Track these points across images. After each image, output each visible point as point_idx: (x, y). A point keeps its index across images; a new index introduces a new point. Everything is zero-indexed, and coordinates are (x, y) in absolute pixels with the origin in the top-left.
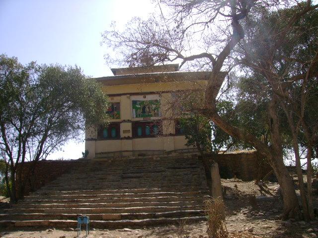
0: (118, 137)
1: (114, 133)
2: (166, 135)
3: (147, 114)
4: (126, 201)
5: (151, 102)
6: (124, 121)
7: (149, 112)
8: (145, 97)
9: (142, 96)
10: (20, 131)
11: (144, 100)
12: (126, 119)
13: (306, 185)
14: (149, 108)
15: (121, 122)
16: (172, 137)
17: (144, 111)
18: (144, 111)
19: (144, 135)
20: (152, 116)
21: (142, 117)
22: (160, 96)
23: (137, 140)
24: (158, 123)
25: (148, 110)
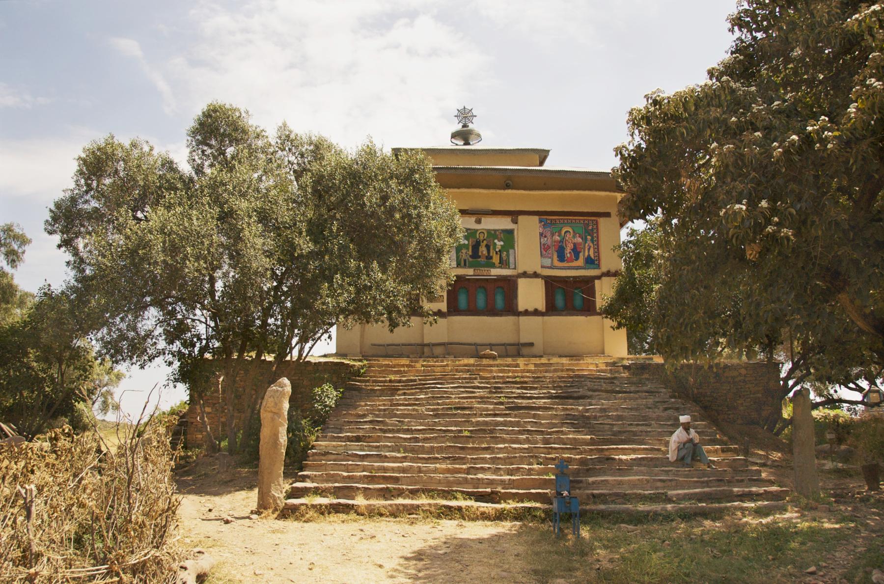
0: (510, 309)
1: (499, 302)
2: (526, 313)
3: (482, 260)
4: (508, 433)
5: (493, 234)
6: (525, 275)
7: (489, 257)
8: (479, 222)
9: (473, 219)
10: (262, 306)
11: (477, 227)
12: (530, 271)
13: (826, 149)
14: (488, 247)
15: (599, 278)
16: (540, 318)
17: (475, 254)
18: (475, 254)
19: (472, 311)
20: (493, 266)
21: (470, 267)
22: (515, 222)
23: (458, 320)
24: (509, 286)
25: (485, 252)
